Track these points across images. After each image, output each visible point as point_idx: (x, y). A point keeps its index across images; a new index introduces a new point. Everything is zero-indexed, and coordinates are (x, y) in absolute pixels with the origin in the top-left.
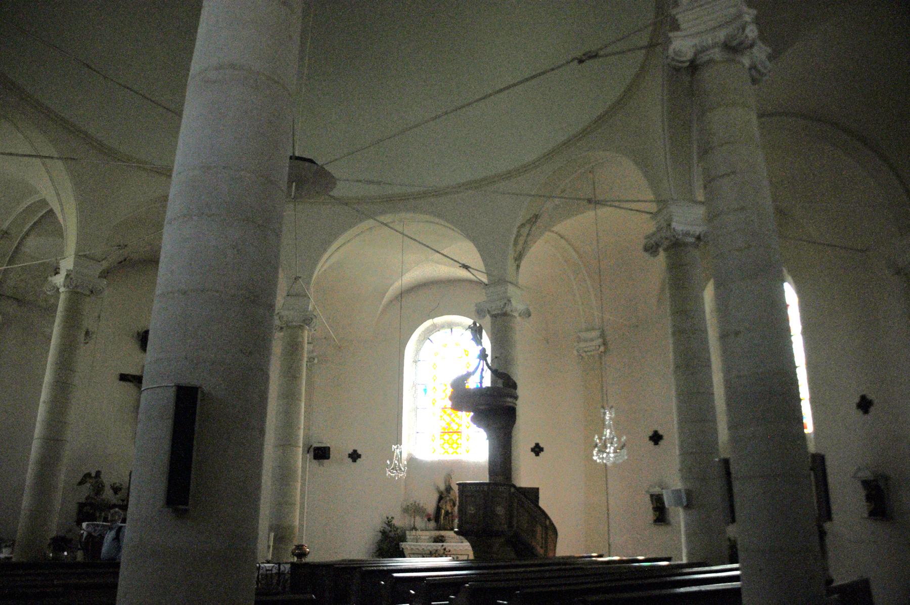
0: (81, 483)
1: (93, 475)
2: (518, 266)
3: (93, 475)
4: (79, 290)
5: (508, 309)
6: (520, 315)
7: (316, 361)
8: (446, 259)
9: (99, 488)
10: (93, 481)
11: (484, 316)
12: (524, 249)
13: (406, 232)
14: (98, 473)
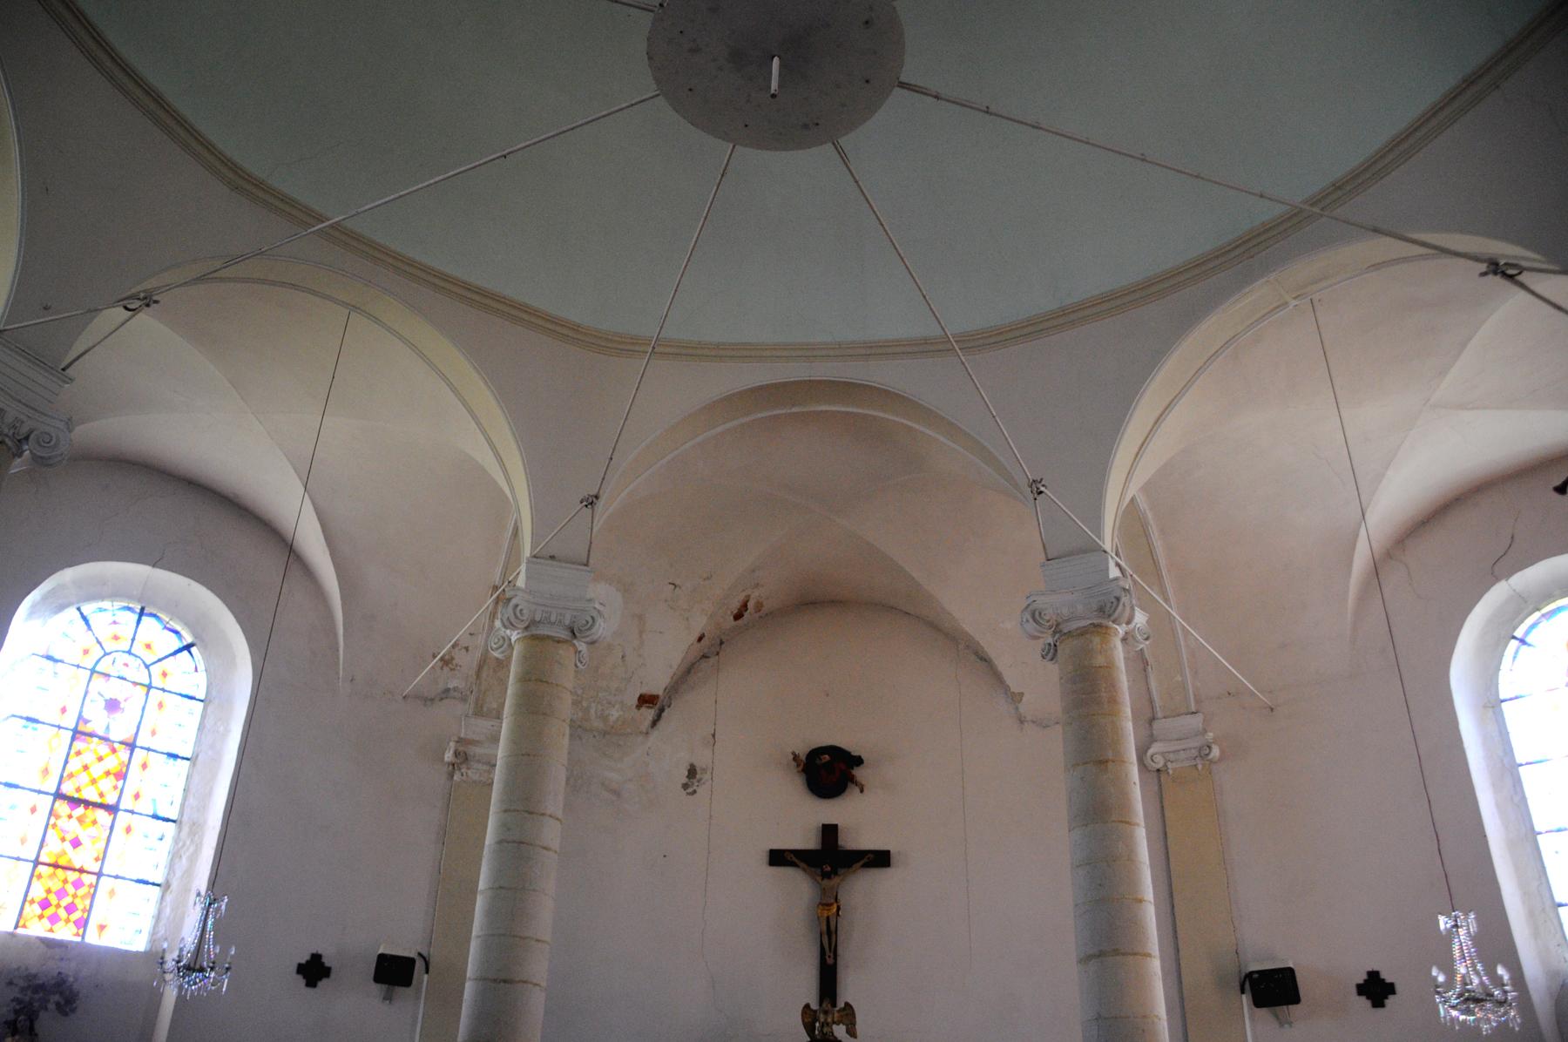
7: (1216, 752)
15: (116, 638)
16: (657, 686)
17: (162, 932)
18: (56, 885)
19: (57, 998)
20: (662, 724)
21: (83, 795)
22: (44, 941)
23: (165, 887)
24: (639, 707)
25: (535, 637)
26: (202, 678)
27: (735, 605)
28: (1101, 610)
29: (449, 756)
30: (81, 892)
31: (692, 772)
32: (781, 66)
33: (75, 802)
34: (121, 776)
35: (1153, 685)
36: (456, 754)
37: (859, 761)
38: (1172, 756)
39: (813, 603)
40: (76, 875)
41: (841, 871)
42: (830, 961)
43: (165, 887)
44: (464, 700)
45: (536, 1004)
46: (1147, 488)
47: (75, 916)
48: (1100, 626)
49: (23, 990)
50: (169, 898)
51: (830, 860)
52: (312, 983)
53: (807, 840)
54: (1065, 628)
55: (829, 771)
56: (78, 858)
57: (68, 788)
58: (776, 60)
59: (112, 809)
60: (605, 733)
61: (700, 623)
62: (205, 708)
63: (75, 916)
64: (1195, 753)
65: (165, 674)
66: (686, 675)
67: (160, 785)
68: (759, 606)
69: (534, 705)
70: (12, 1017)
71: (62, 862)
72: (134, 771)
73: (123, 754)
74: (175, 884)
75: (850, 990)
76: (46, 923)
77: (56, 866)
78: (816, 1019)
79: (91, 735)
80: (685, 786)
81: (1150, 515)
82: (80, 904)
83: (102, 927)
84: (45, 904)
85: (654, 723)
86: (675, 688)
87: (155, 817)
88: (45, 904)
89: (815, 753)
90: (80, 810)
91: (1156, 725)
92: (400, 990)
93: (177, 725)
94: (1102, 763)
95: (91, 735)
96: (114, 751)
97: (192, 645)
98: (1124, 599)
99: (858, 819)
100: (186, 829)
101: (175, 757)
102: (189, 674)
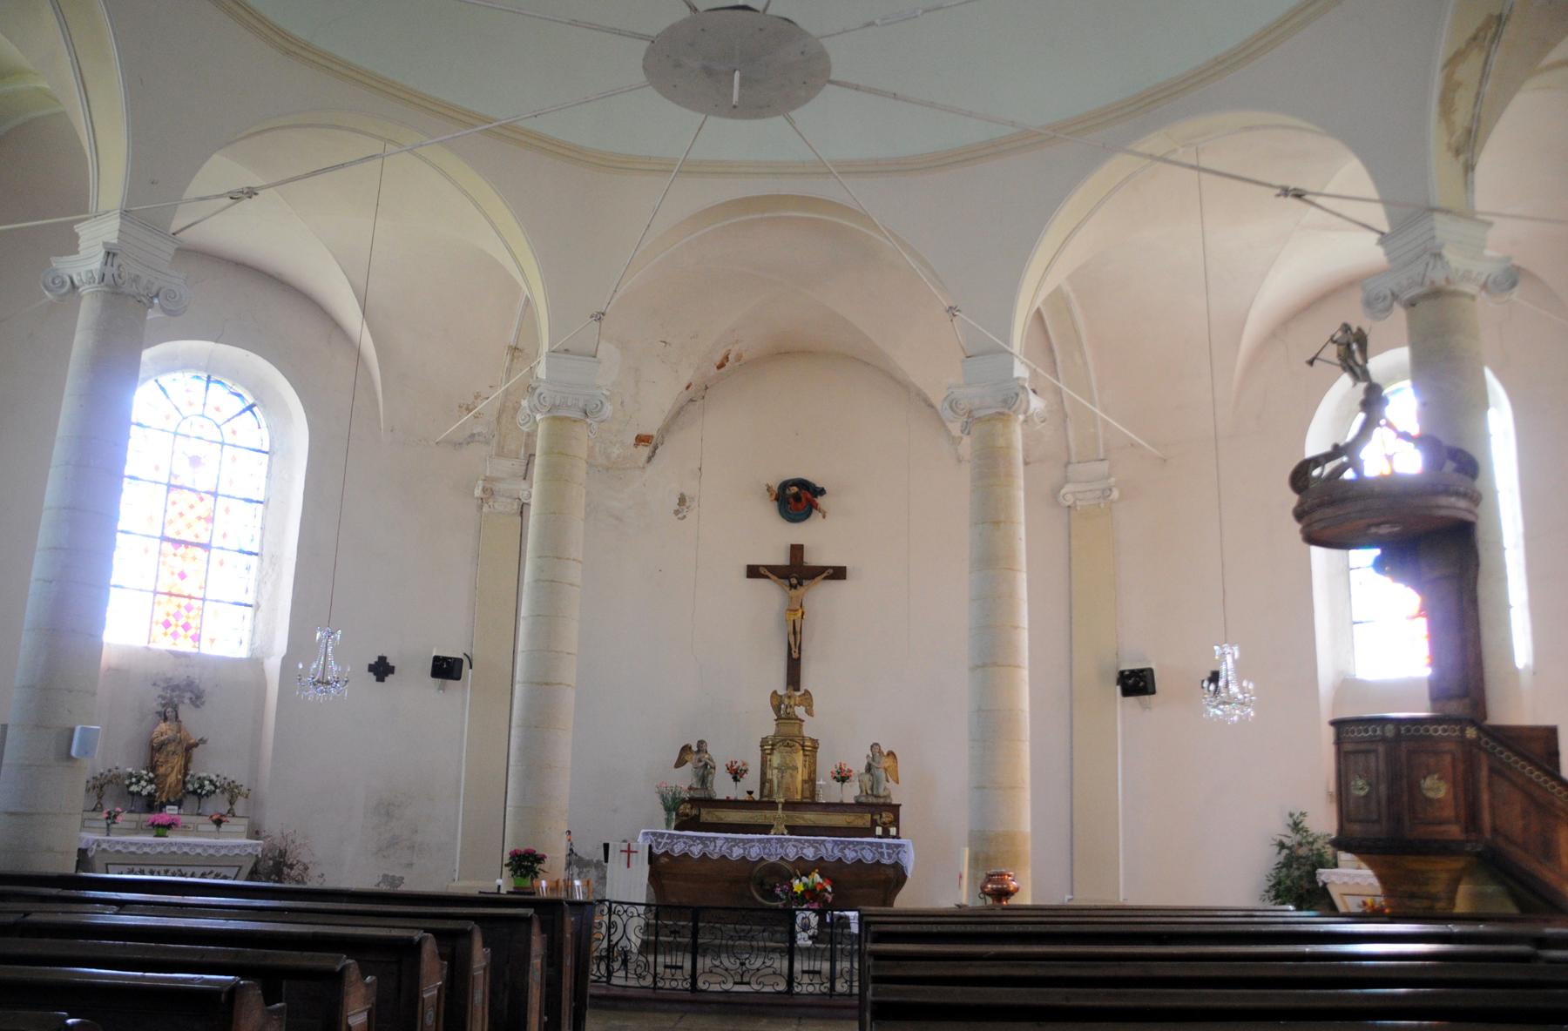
0: (680, 763)
1: (695, 748)
2: (1469, 168)
3: (695, 748)
4: (562, 413)
5: (1438, 276)
6: (1484, 287)
7: (1115, 494)
8: (1335, 220)
9: (705, 773)
10: (695, 757)
11: (1389, 309)
12: (1476, 119)
13: (1205, 162)
14: (701, 743)
15: (191, 404)
16: (651, 429)
17: (258, 643)
18: (173, 610)
19: (188, 695)
20: (655, 461)
21: (183, 537)
22: (171, 652)
23: (256, 607)
24: (636, 445)
25: (555, 418)
26: (265, 433)
27: (718, 359)
28: (1005, 401)
29: (478, 492)
30: (192, 614)
31: (682, 500)
32: (742, 78)
33: (177, 543)
34: (210, 520)
35: (1071, 434)
36: (484, 490)
37: (822, 492)
38: (1080, 496)
39: (787, 353)
40: (184, 602)
41: (806, 583)
42: (795, 655)
43: (256, 607)
44: (487, 443)
45: (569, 698)
46: (1045, 302)
47: (191, 632)
48: (1002, 414)
49: (164, 689)
50: (259, 614)
51: (796, 572)
52: (381, 679)
53: (782, 559)
54: (977, 414)
55: (798, 499)
56: (185, 587)
57: (170, 533)
58: (737, 74)
59: (206, 547)
60: (608, 469)
61: (687, 376)
62: (270, 460)
63: (191, 632)
64: (1099, 493)
65: (234, 432)
66: (678, 414)
67: (242, 525)
68: (739, 357)
69: (557, 476)
70: (160, 709)
71: (174, 591)
72: (220, 516)
73: (209, 499)
74: (263, 605)
75: (809, 681)
76: (169, 638)
77: (170, 594)
78: (781, 702)
79: (181, 487)
80: (677, 512)
81: (1072, 296)
82: (194, 623)
83: (212, 641)
84: (167, 624)
85: (649, 459)
86: (666, 429)
87: (241, 551)
88: (167, 624)
89: (785, 485)
90: (182, 549)
91: (1070, 468)
92: (450, 682)
93: (250, 475)
94: (997, 523)
95: (181, 487)
96: (202, 499)
97: (253, 405)
98: (1022, 396)
99: (820, 540)
100: (267, 560)
101: (251, 501)
102: (253, 431)
